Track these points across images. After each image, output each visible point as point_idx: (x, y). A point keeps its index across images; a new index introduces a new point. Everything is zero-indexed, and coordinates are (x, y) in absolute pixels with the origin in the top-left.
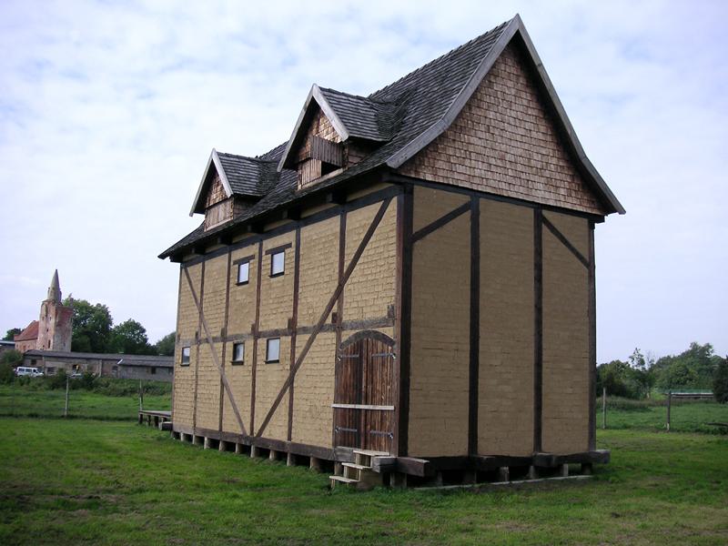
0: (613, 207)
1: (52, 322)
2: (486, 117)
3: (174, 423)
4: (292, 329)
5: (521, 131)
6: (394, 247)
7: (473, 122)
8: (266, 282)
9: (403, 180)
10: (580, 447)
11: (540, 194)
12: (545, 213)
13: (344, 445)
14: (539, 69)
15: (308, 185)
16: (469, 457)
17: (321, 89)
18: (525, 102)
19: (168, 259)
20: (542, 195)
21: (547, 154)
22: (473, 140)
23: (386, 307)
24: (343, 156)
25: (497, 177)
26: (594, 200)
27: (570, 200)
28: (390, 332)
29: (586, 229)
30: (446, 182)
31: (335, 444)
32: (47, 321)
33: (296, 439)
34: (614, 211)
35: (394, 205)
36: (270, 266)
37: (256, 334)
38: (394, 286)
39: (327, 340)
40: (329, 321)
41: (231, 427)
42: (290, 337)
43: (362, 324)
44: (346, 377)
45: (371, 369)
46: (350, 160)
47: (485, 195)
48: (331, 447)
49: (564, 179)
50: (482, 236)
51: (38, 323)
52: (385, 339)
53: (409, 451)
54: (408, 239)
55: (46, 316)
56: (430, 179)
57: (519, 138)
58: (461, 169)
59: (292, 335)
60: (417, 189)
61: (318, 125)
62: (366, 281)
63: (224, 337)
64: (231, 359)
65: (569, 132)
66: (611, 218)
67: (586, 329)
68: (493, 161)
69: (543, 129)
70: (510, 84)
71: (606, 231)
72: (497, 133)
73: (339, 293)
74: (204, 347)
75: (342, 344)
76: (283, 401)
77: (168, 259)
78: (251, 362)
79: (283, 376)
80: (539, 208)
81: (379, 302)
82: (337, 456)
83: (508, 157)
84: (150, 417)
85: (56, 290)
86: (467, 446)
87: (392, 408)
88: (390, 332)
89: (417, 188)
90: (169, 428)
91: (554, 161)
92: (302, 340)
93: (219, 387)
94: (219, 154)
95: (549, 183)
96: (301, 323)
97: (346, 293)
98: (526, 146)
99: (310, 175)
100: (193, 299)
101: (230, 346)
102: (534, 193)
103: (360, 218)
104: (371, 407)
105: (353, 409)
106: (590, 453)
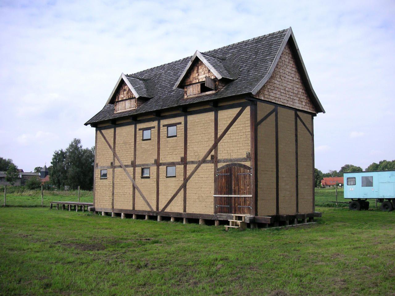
0: (321, 110)
2: (279, 72)
3: (96, 207)
4: (184, 161)
5: (290, 78)
6: (249, 127)
7: (275, 74)
8: (163, 140)
9: (254, 99)
10: (310, 211)
11: (297, 105)
12: (299, 113)
13: (222, 213)
14: (298, 51)
15: (191, 96)
16: (277, 216)
17: (202, 53)
18: (291, 65)
19: (89, 125)
20: (298, 106)
21: (298, 88)
22: (276, 82)
23: (245, 153)
24: (215, 85)
25: (284, 98)
26: (314, 107)
27: (306, 107)
28: (248, 164)
29: (311, 119)
30: (268, 100)
31: (216, 212)
33: (189, 211)
34: (322, 112)
35: (248, 110)
36: (166, 133)
37: (158, 164)
38: (250, 144)
40: (209, 158)
42: (183, 166)
43: (231, 160)
44: (221, 183)
45: (238, 180)
46: (219, 87)
47: (280, 106)
48: (213, 214)
49: (304, 97)
50: (279, 123)
52: (245, 167)
53: (258, 214)
54: (255, 124)
56: (263, 99)
57: (290, 81)
58: (272, 94)
59: (183, 164)
60: (259, 103)
61: (198, 70)
62: (233, 142)
63: (134, 165)
64: (140, 175)
65: (308, 78)
66: (319, 115)
67: (311, 161)
68: (282, 91)
69: (297, 77)
70: (287, 57)
71: (318, 119)
72: (283, 79)
73: (215, 146)
74: (118, 170)
75: (218, 169)
76: (179, 194)
77: (89, 125)
78: (155, 176)
79: (179, 183)
80: (296, 110)
81: (241, 151)
82: (218, 218)
83: (287, 89)
84: (64, 205)
86: (276, 211)
87: (251, 196)
89: (258, 103)
90: (93, 210)
91: (301, 90)
92: (190, 168)
93: (132, 189)
94: (127, 76)
95: (300, 101)
96: (189, 159)
98: (292, 84)
99: (193, 92)
100: (108, 146)
101: (138, 170)
102: (295, 104)
103: (226, 116)
104: (239, 196)
105: (226, 197)
106: (313, 213)
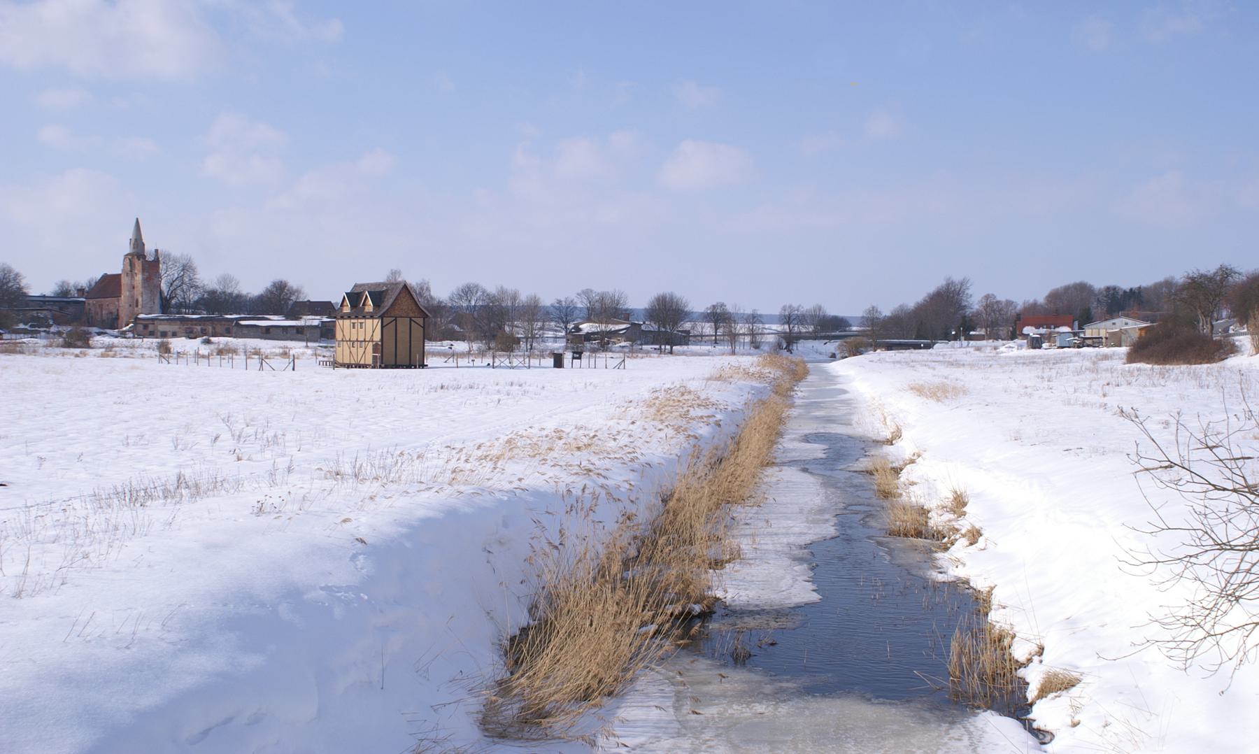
1: (139, 278)
32: (132, 277)
39: (371, 344)
41: (345, 362)
51: (117, 278)
55: (131, 272)
85: (138, 242)
88: (380, 343)
97: (371, 331)
